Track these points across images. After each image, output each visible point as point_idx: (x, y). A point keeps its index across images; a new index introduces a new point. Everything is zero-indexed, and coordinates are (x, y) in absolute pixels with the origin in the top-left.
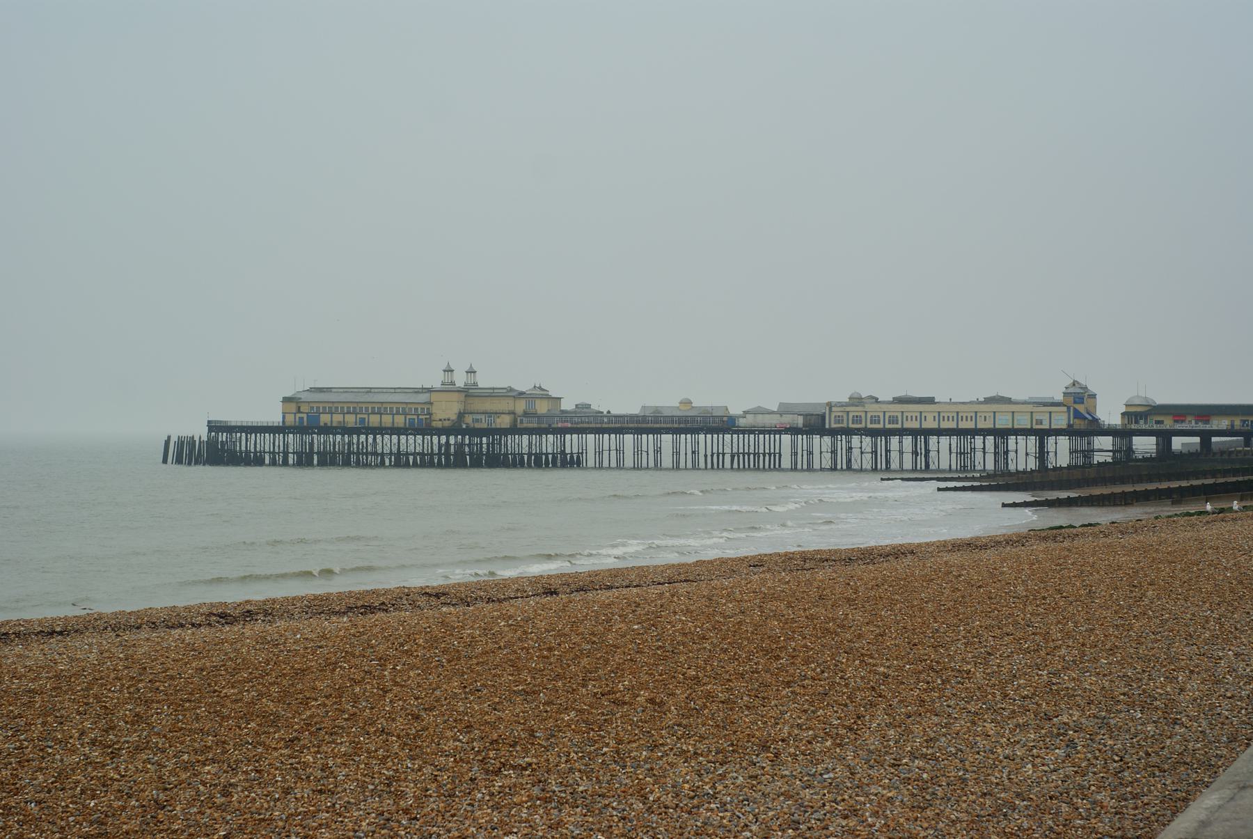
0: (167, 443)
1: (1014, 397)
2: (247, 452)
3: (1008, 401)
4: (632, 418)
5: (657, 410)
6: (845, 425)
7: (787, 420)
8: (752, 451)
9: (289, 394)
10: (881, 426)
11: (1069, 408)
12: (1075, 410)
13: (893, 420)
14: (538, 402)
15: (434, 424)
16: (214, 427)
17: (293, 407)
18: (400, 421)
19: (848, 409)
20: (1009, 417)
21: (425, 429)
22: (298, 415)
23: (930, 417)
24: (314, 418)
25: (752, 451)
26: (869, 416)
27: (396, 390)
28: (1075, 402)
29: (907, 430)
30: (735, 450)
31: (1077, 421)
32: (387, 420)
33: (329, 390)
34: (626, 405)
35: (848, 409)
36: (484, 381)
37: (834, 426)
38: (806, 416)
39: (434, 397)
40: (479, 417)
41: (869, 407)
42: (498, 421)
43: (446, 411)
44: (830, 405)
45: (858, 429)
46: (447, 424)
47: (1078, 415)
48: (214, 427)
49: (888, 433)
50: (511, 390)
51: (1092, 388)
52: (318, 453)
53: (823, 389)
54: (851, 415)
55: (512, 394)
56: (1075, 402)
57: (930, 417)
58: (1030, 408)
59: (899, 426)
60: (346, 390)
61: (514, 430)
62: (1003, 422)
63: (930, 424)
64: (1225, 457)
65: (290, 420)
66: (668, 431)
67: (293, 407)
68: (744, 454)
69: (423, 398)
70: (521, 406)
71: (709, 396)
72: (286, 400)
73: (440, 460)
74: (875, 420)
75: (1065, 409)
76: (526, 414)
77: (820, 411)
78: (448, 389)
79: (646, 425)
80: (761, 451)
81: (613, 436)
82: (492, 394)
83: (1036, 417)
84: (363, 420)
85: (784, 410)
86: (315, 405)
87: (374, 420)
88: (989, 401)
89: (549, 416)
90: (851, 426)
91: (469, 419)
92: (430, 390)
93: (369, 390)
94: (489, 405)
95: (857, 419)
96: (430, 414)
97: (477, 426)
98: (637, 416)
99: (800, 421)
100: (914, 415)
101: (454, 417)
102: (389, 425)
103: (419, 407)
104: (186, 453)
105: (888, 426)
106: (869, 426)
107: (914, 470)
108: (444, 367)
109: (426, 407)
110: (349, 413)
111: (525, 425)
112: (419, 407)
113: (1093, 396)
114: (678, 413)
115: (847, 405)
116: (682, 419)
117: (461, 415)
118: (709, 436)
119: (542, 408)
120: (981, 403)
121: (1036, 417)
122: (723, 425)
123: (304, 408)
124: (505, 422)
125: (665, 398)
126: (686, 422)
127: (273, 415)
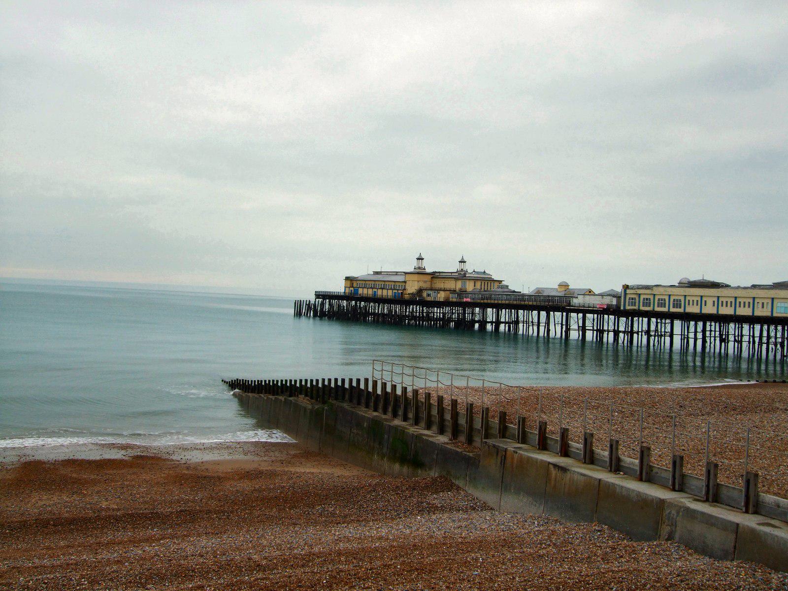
2: (680, 366)
6: (636, 308)
9: (460, 260)
13: (677, 304)
16: (318, 295)
23: (710, 302)
33: (247, 295)
35: (639, 292)
37: (628, 308)
39: (408, 277)
41: (656, 291)
42: (439, 295)
43: (412, 288)
45: (647, 312)
48: (318, 295)
54: (642, 297)
57: (710, 302)
59: (681, 310)
63: (709, 309)
72: (347, 279)
74: (662, 304)
78: (420, 272)
81: (653, 320)
90: (642, 308)
91: (425, 294)
95: (647, 302)
96: (405, 289)
97: (429, 299)
100: (695, 299)
108: (417, 256)
109: (403, 284)
117: (420, 291)
126: (549, 301)
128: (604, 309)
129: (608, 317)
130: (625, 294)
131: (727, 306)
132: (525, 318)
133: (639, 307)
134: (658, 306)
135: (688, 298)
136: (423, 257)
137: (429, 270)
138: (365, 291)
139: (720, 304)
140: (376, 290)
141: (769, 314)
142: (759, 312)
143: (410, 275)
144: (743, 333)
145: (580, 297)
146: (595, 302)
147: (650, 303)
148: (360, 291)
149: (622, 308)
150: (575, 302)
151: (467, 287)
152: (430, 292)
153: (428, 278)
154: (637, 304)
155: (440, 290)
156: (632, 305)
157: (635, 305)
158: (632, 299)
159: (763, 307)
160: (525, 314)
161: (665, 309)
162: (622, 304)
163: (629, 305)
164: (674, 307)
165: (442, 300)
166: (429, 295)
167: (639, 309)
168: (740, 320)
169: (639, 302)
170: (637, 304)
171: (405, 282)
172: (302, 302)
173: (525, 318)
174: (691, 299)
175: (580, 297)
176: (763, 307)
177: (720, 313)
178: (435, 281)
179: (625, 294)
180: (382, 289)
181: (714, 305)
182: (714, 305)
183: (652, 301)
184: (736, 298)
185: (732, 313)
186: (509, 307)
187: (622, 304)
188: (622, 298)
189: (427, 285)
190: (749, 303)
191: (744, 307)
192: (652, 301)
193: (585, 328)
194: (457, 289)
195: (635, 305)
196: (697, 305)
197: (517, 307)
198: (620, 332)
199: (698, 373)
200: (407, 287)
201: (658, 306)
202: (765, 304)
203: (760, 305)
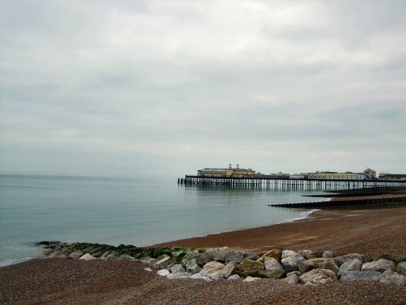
0: (179, 179)
1: (353, 172)
3: (351, 173)
4: (268, 176)
5: (274, 174)
6: (312, 178)
7: (300, 177)
8: (293, 184)
11: (365, 175)
12: (367, 176)
13: (324, 177)
14: (248, 172)
15: (227, 176)
16: (186, 176)
17: (200, 172)
18: (220, 176)
19: (313, 174)
20: (351, 177)
21: (225, 178)
23: (332, 177)
24: (203, 175)
25: (293, 184)
26: (318, 176)
27: (221, 169)
28: (367, 173)
29: (335, 180)
32: (217, 175)
33: (208, 169)
34: (267, 173)
35: (313, 174)
36: (240, 167)
37: (310, 178)
38: (304, 176)
39: (227, 171)
40: (236, 175)
42: (240, 176)
43: (229, 174)
44: (309, 173)
46: (229, 176)
47: (367, 177)
48: (186, 176)
49: (322, 180)
50: (244, 169)
51: (375, 170)
52: (381, 185)
53: (306, 171)
54: (314, 176)
55: (245, 170)
57: (332, 177)
58: (356, 175)
59: (325, 179)
60: (211, 169)
61: (243, 178)
62: (349, 178)
63: (332, 178)
64: (387, 188)
65: (199, 175)
66: (274, 179)
67: (200, 172)
69: (225, 171)
70: (245, 173)
71: (285, 171)
72: (198, 171)
74: (319, 177)
75: (364, 175)
76: (246, 175)
77: (307, 175)
78: (230, 169)
81: (258, 180)
82: (240, 170)
84: (213, 175)
85: (302, 174)
86: (204, 172)
87: (215, 175)
88: (346, 173)
89: (251, 175)
90: (314, 178)
91: (234, 175)
92: (226, 169)
93: (216, 169)
94: (239, 173)
95: (315, 177)
96: (226, 174)
98: (269, 175)
99: (303, 177)
100: (328, 176)
101: (230, 175)
102: (218, 177)
103: (224, 173)
106: (318, 178)
107: (318, 190)
108: (229, 164)
109: (225, 173)
110: (220, 174)
111: (245, 177)
112: (224, 173)
113: (375, 172)
114: (279, 175)
116: (279, 176)
117: (232, 175)
119: (249, 173)
120: (345, 173)
121: (357, 177)
122: (285, 178)
123: (202, 173)
124: (241, 176)
125: (276, 172)
126: (279, 177)
127: (196, 174)
130: (309, 175)
135: (326, 176)
136: (231, 164)
137: (233, 168)
142: (344, 179)
145: (292, 176)
149: (308, 178)
150: (291, 177)
153: (233, 171)
160: (283, 181)
161: (321, 179)
168: (330, 180)
171: (226, 172)
172: (194, 186)
174: (332, 176)
175: (292, 176)
178: (235, 171)
179: (309, 175)
184: (330, 175)
186: (259, 179)
193: (362, 189)
197: (253, 179)
199: (295, 191)
200: (227, 173)
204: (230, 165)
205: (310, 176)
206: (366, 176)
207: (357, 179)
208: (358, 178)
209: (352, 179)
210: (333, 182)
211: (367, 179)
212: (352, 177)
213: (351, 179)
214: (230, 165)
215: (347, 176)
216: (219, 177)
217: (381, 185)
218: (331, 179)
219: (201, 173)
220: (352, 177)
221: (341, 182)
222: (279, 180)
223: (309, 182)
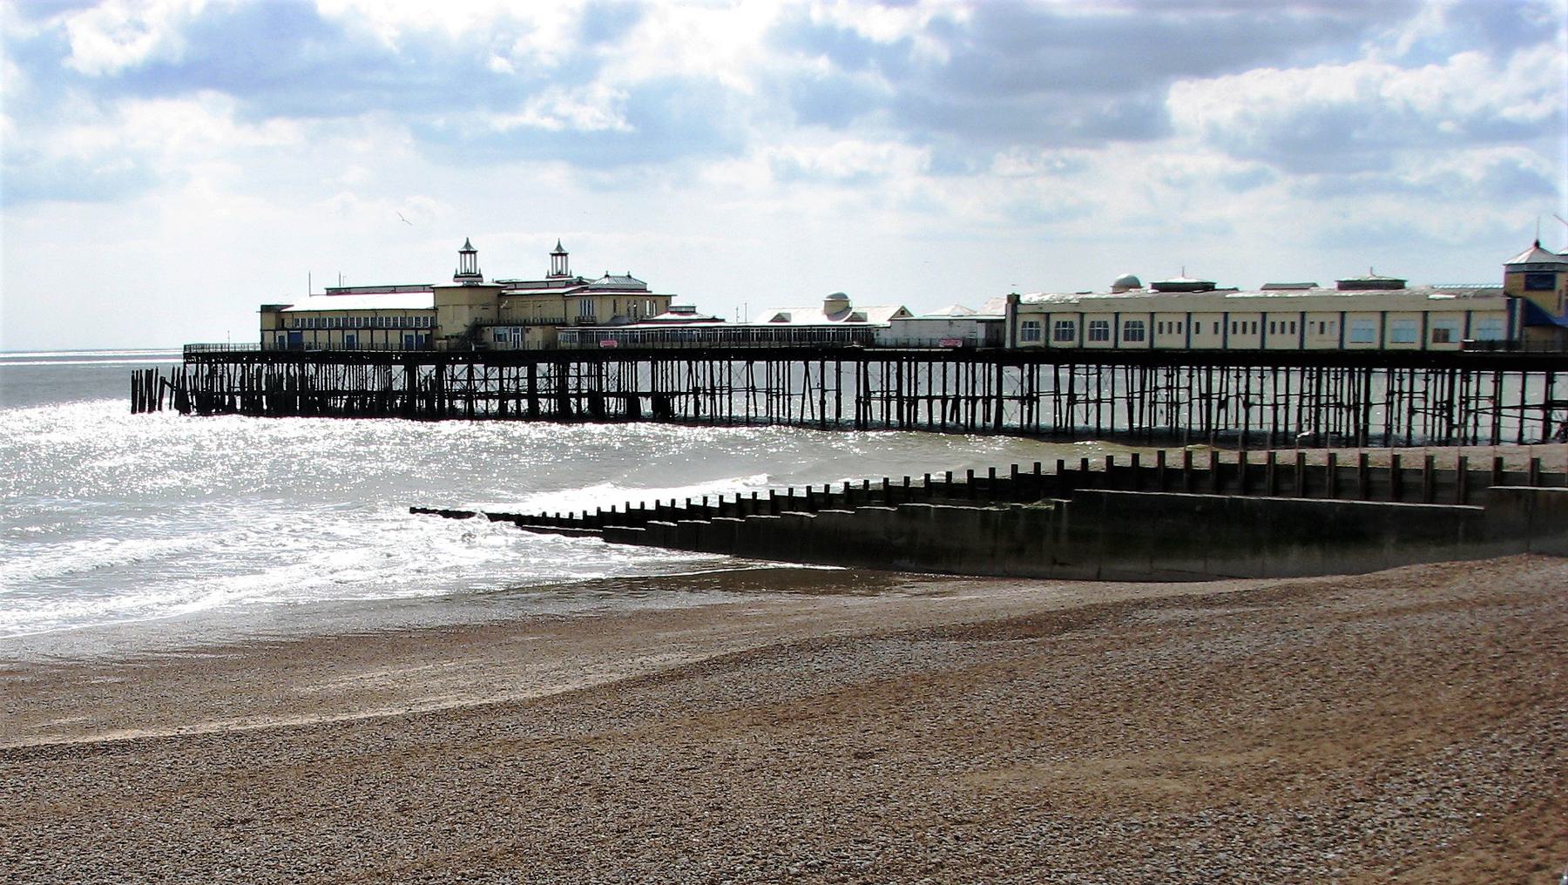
6: (1041, 343)
10: (1109, 344)
13: (1134, 332)
22: (279, 333)
28: (1528, 287)
29: (1161, 351)
30: (951, 392)
31: (1534, 334)
37: (1021, 344)
42: (528, 337)
43: (455, 324)
56: (1528, 287)
59: (1144, 344)
62: (1362, 336)
67: (272, 317)
68: (967, 398)
69: (425, 301)
72: (266, 309)
73: (233, 401)
74: (1100, 332)
79: (780, 345)
80: (1332, 410)
83: (1435, 323)
91: (489, 335)
92: (434, 289)
96: (434, 327)
97: (500, 346)
104: (204, 384)
105: (1123, 344)
106: (1088, 344)
108: (461, 247)
115: (264, 355)
117: (476, 329)
118: (716, 363)
121: (1435, 323)
127: (247, 334)
128: (955, 348)
129: (807, 365)
131: (1283, 331)
132: (1429, 429)
133: (1047, 341)
134: (1091, 338)
135: (1158, 319)
137: (487, 281)
138: (322, 336)
139: (1297, 328)
140: (354, 333)
141: (1336, 345)
142: (1314, 342)
143: (1346, 326)
144: (1373, 400)
146: (933, 336)
147: (1072, 332)
148: (308, 337)
149: (1008, 345)
151: (597, 313)
152: (501, 330)
154: (1042, 335)
155: (534, 325)
156: (1030, 339)
157: (1037, 338)
158: (1031, 324)
159: (1322, 331)
161: (1108, 344)
162: (1008, 335)
163: (1023, 339)
164: (1126, 339)
165: (533, 347)
166: (499, 337)
167: (1047, 346)
169: (1047, 331)
170: (1042, 335)
173: (1429, 429)
176: (1322, 331)
177: (1230, 346)
180: (372, 329)
181: (1216, 332)
182: (1216, 332)
183: (1077, 327)
184: (1264, 314)
185: (1257, 346)
187: (1008, 335)
188: (1008, 323)
189: (488, 315)
190: (1293, 324)
191: (1283, 331)
192: (1077, 327)
194: (571, 319)
195: (1037, 338)
196: (1179, 331)
198: (609, 394)
201: (1091, 338)
202: (1327, 326)
203: (1317, 327)
204: (560, 253)
205: (1020, 320)
206: (1518, 312)
207: (1435, 340)
208: (1443, 336)
209: (1388, 346)
210: (1295, 378)
211: (1538, 339)
212: (1342, 335)
213: (1375, 346)
214: (560, 253)
215: (1337, 318)
216: (334, 353)
217: (1223, 412)
218: (1194, 345)
219: (283, 329)
220: (1342, 335)
221: (1106, 373)
222: (797, 366)
223: (1203, 375)
